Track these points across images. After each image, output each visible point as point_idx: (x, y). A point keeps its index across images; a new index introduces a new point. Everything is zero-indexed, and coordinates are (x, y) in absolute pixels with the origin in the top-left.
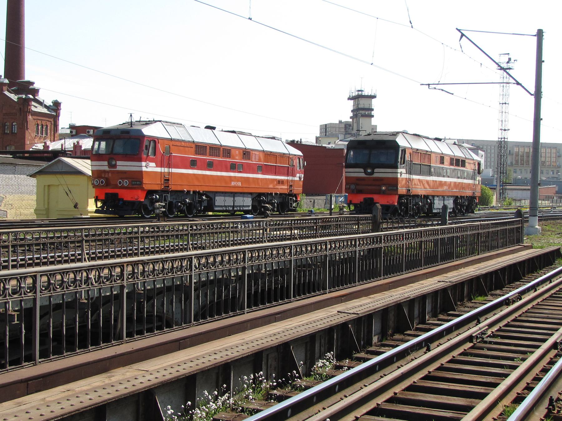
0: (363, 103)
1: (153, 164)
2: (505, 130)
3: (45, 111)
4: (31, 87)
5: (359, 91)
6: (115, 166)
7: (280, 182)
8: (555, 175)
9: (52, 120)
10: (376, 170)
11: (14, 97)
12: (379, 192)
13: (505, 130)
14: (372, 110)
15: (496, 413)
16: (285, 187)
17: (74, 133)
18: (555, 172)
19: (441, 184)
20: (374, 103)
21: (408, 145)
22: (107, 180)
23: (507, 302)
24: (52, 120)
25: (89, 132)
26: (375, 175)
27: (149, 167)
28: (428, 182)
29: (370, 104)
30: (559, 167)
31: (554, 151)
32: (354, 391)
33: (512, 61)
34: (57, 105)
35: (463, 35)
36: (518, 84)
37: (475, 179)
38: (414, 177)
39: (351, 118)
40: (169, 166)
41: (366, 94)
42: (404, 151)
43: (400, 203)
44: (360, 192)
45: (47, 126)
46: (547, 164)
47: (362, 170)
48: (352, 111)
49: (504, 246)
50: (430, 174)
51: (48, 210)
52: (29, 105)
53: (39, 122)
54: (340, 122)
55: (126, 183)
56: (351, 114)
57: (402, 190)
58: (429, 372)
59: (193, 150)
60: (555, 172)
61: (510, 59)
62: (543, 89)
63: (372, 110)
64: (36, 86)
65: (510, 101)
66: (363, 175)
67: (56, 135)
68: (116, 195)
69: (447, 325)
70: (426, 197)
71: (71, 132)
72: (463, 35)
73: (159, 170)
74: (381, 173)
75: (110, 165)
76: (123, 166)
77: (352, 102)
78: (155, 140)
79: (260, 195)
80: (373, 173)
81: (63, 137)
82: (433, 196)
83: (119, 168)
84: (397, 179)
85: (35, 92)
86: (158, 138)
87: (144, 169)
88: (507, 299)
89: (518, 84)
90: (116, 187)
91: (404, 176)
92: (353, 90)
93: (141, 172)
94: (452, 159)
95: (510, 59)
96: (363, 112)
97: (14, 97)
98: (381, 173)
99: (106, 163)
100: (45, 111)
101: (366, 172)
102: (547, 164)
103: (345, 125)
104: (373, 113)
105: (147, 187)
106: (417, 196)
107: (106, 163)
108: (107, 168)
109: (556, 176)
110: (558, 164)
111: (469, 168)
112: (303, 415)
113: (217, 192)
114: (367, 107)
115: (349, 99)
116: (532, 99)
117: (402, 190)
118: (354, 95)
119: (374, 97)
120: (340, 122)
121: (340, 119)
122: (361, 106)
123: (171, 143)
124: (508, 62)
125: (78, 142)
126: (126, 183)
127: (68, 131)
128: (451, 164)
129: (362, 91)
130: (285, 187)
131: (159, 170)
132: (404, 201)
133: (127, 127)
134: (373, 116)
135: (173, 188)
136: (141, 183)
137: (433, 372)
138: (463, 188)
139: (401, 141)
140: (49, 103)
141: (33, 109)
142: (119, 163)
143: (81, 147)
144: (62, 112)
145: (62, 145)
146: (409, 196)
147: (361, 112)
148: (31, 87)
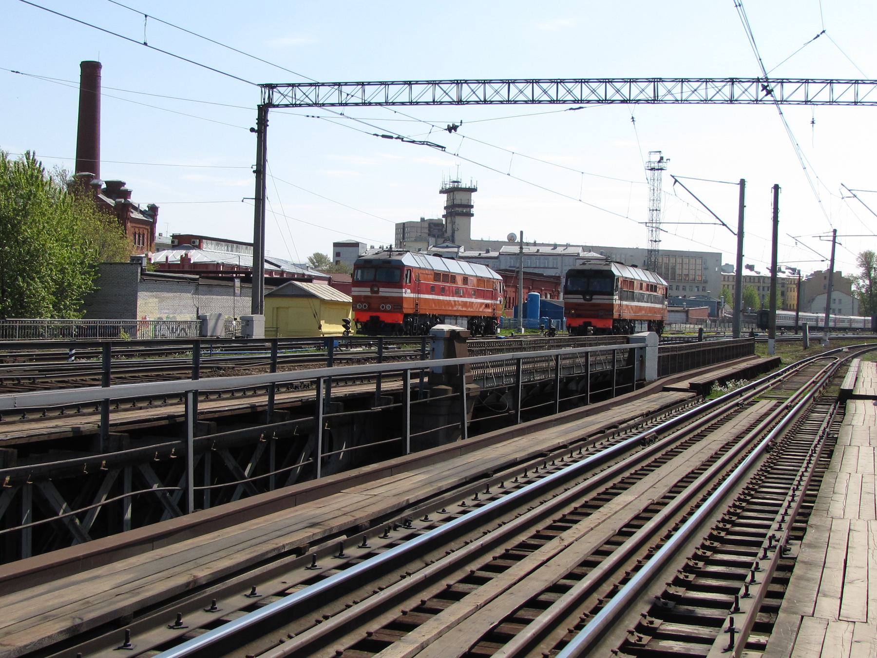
0: (459, 198)
1: (409, 291)
2: (655, 241)
3: (140, 217)
4: (122, 188)
5: (454, 182)
6: (378, 292)
7: (487, 306)
8: (701, 293)
9: (148, 227)
10: (594, 297)
11: (111, 202)
12: (596, 317)
13: (655, 241)
14: (472, 207)
15: (545, 647)
16: (490, 310)
17: (176, 243)
18: (701, 289)
19: (641, 308)
20: (475, 198)
21: (646, 279)
22: (369, 305)
23: (643, 442)
24: (148, 227)
25: (194, 242)
26: (594, 301)
27: (407, 294)
28: (632, 307)
29: (469, 200)
30: (706, 282)
31: (699, 261)
32: (302, 629)
33: (665, 160)
34: (153, 210)
35: (676, 181)
36: (724, 224)
37: (663, 304)
38: (625, 303)
39: (444, 216)
40: (419, 292)
41: (464, 186)
42: (618, 279)
43: (406, 323)
44: (578, 316)
45: (144, 235)
46: (691, 277)
47: (581, 297)
48: (445, 208)
49: (713, 362)
50: (633, 299)
51: (277, 330)
52: (128, 211)
53: (137, 230)
54: (423, 220)
55: (388, 307)
56: (444, 212)
57: (616, 315)
58: (370, 634)
59: (432, 277)
60: (701, 289)
61: (662, 158)
62: (745, 230)
63: (472, 207)
64: (127, 187)
65: (662, 206)
66: (582, 301)
67: (153, 245)
68: (378, 317)
69: (549, 478)
70: (631, 321)
71: (172, 242)
72: (676, 181)
73: (412, 295)
74: (598, 299)
75: (372, 291)
76: (384, 292)
77: (445, 196)
78: (410, 269)
79: (473, 318)
80: (591, 299)
81: (160, 247)
82: (635, 320)
83: (381, 294)
84: (613, 304)
85: (127, 194)
86: (413, 267)
87: (404, 295)
88: (643, 438)
89: (724, 224)
90: (378, 310)
91: (618, 302)
92: (447, 180)
93: (402, 298)
94: (648, 285)
95: (662, 158)
96: (460, 210)
97: (111, 202)
98: (598, 299)
99: (369, 289)
100: (140, 217)
101: (584, 299)
102: (691, 277)
103: (429, 224)
104: (473, 211)
105: (405, 311)
106: (625, 320)
107: (369, 289)
108: (369, 294)
109: (705, 294)
110: (704, 278)
111: (660, 293)
112: (252, 649)
113: (445, 316)
114: (464, 202)
115: (442, 192)
116: (736, 238)
117: (616, 315)
118: (448, 187)
119: (475, 190)
120: (423, 220)
121: (423, 216)
122: (457, 202)
123: (420, 271)
124: (659, 162)
125: (186, 255)
126: (388, 307)
127: (170, 242)
128: (647, 290)
129: (458, 182)
130: (490, 310)
131: (412, 295)
132: (410, 319)
133: (384, 256)
134: (472, 215)
135: (422, 312)
136: (402, 307)
137: (376, 632)
138: (655, 313)
139: (616, 270)
140: (144, 207)
141: (133, 215)
142: (381, 289)
143: (190, 260)
144: (159, 218)
145: (167, 258)
146: (620, 320)
147: (457, 209)
148: (122, 188)
